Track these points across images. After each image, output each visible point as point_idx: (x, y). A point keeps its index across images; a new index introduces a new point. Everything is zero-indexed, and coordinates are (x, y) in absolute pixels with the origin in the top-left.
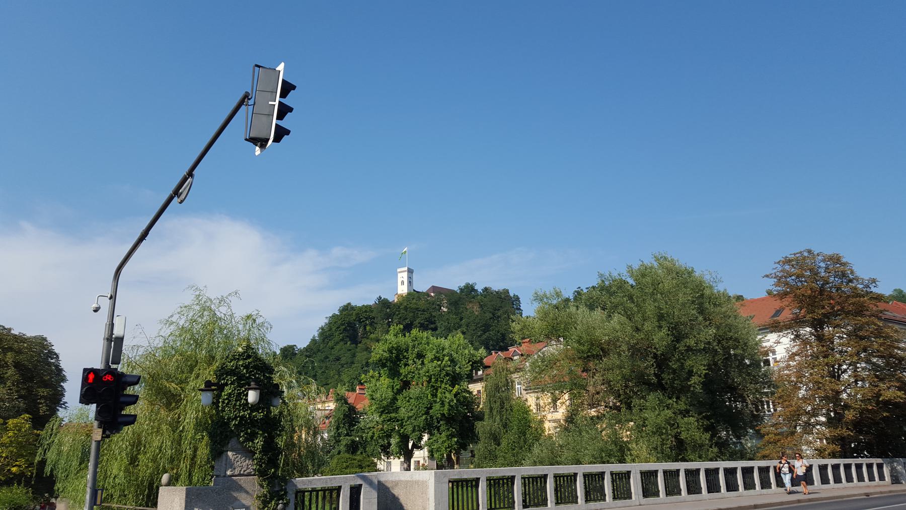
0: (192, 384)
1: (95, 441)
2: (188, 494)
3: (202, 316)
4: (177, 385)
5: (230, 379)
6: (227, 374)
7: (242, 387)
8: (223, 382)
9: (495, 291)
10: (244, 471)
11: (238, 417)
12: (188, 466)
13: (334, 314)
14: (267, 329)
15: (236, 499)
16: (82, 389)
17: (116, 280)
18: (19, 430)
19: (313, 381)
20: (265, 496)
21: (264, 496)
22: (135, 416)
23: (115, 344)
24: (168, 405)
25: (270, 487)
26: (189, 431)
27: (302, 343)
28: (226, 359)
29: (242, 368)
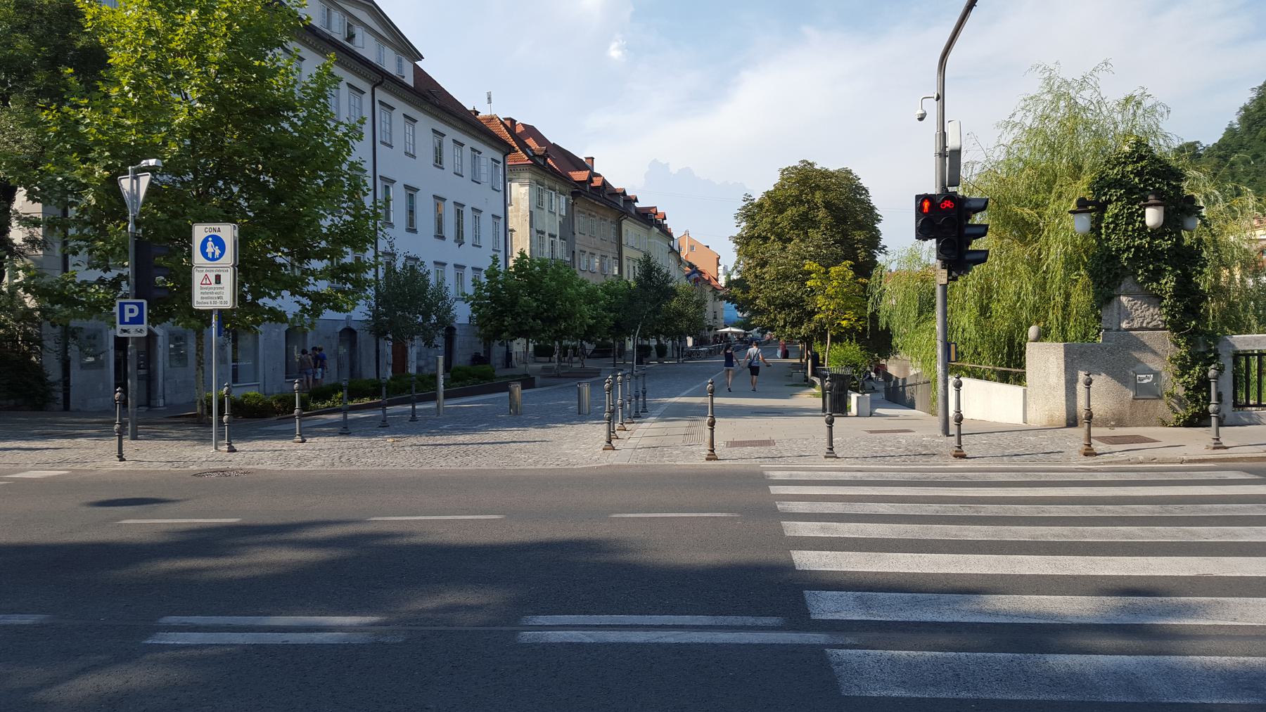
0: (1052, 207)
1: (940, 285)
2: (1068, 353)
3: (1054, 110)
4: (1032, 209)
5: (1115, 193)
6: (1110, 186)
7: (1135, 204)
8: (1104, 198)
10: (1148, 323)
11: (1132, 248)
12: (1060, 319)
14: (1162, 116)
15: (1138, 361)
16: (916, 222)
17: (942, 73)
18: (843, 279)
19: (1249, 190)
20: (1184, 358)
21: (1181, 359)
22: (987, 252)
23: (951, 159)
24: (1022, 239)
25: (1191, 346)
26: (1056, 272)
27: (1210, 137)
28: (1106, 165)
29: (1132, 176)
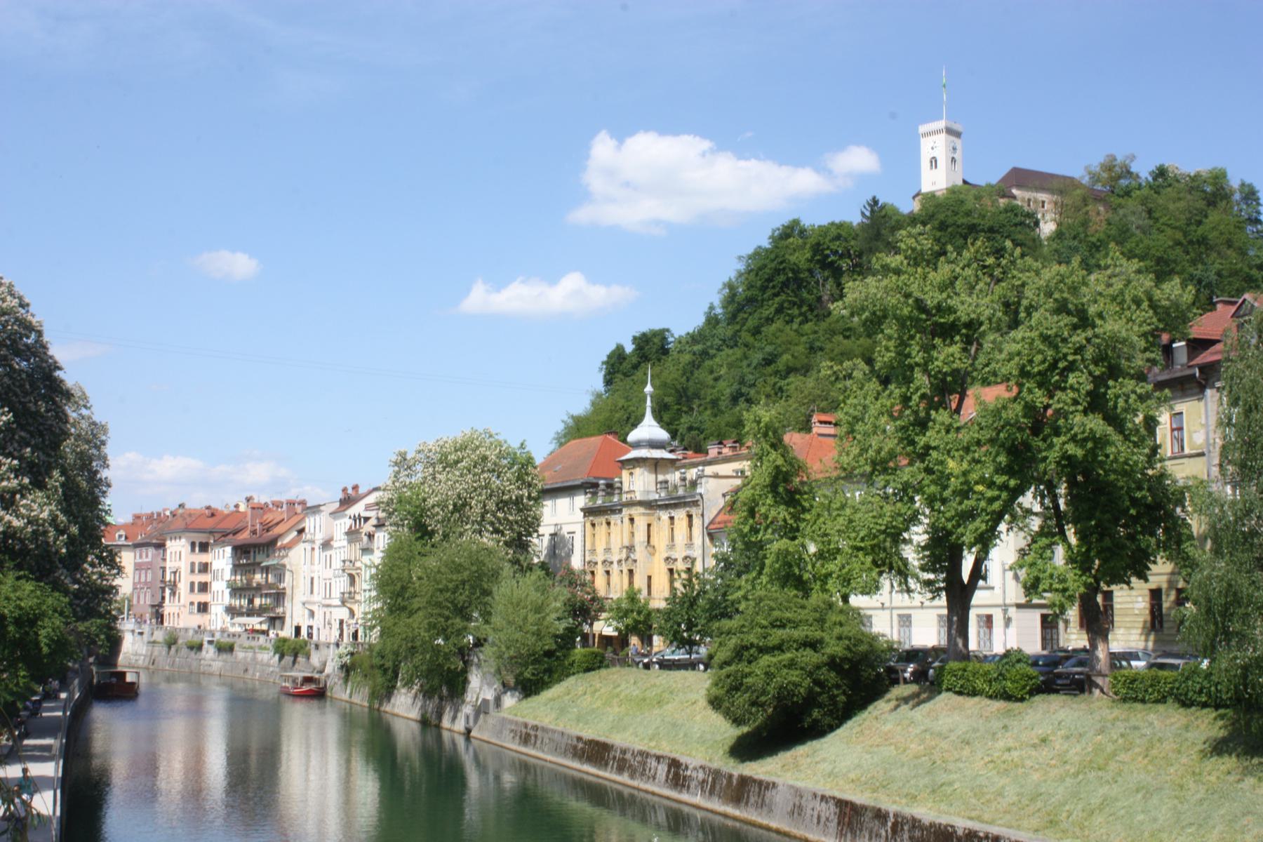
9: (1189, 176)
13: (760, 247)
